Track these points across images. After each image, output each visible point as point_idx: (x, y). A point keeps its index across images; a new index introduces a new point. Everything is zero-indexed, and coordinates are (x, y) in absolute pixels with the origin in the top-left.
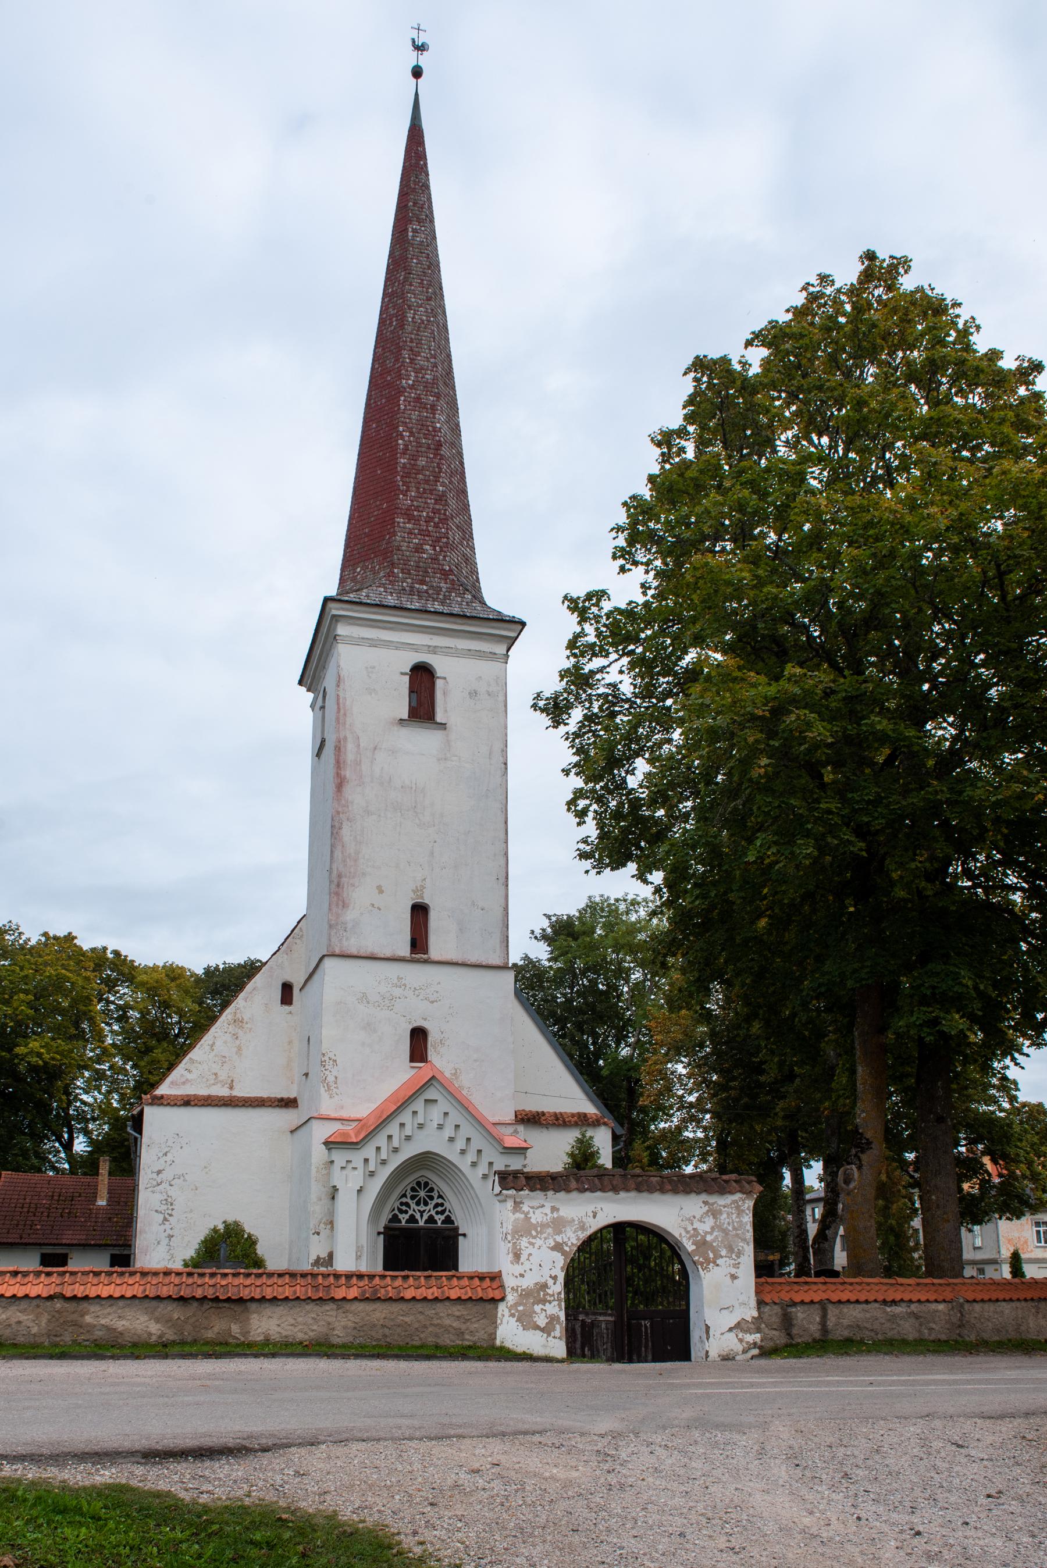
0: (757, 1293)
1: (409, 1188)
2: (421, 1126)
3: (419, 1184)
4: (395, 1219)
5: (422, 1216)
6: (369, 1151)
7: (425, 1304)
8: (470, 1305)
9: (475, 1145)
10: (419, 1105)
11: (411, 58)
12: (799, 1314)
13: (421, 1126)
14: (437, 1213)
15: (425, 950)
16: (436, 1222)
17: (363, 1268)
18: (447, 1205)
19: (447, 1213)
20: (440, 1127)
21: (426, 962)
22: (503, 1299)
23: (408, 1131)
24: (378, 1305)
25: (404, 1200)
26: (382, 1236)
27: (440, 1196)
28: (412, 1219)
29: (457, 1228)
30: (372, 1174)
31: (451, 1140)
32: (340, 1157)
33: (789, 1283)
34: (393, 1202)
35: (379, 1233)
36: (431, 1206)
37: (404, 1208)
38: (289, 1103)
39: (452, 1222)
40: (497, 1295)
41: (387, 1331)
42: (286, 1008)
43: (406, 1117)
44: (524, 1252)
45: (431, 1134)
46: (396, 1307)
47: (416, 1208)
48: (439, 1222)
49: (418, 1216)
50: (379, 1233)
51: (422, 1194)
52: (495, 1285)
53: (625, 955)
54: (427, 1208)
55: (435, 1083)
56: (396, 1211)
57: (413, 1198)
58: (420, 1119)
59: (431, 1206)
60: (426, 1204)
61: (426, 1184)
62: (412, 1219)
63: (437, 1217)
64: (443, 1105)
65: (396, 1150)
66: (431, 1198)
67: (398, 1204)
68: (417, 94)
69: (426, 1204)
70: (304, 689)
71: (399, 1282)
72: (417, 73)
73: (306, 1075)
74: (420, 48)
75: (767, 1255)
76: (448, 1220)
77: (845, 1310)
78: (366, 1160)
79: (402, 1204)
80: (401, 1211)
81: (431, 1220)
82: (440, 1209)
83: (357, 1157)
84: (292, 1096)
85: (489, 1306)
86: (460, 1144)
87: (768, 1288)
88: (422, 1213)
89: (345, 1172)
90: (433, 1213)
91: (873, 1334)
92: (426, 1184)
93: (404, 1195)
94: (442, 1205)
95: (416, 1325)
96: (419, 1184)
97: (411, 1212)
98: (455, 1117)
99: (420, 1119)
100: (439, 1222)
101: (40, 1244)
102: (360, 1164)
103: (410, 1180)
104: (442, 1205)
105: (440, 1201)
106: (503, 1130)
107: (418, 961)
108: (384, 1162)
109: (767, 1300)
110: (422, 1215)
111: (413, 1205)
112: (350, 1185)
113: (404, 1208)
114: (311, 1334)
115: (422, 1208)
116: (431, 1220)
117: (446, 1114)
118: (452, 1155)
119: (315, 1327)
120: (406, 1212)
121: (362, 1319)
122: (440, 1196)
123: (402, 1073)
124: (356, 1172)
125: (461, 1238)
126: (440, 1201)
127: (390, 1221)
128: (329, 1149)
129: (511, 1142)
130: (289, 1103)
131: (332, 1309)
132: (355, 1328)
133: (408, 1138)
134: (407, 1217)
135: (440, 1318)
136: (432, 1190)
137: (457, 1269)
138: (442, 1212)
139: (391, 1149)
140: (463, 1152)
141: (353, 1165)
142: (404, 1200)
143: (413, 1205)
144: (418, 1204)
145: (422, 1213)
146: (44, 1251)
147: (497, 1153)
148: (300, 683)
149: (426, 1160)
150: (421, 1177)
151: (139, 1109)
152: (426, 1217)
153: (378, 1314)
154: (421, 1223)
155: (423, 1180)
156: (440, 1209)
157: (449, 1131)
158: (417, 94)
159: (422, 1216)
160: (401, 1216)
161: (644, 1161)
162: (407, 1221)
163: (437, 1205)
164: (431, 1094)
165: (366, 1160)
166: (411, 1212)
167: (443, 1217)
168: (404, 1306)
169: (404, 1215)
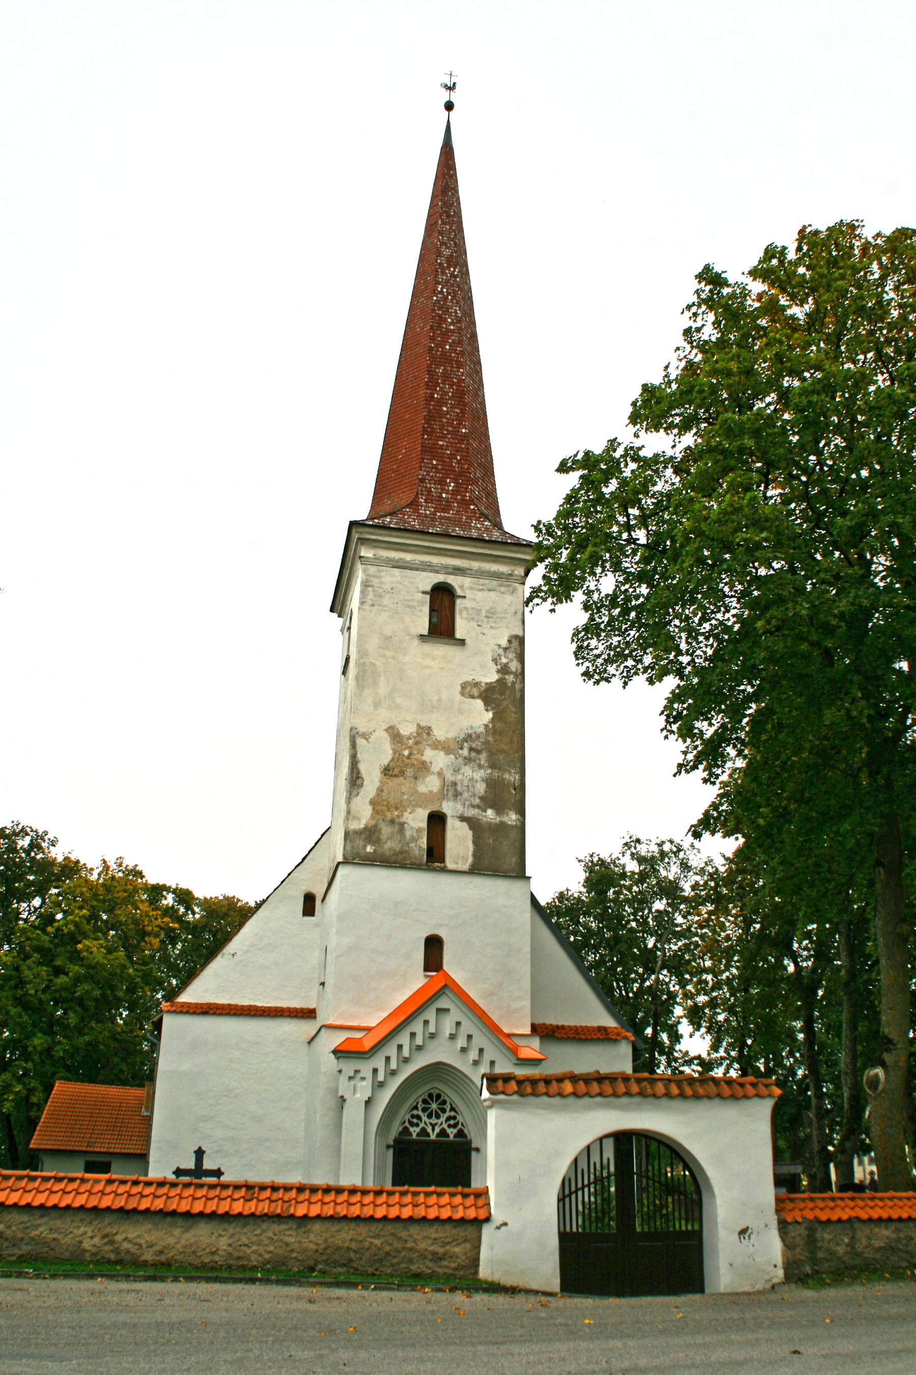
0: (778, 1211)
1: (420, 1100)
2: (432, 1036)
3: (430, 1096)
4: (406, 1131)
5: (433, 1130)
6: (378, 1062)
7: (399, 1225)
8: (448, 1227)
9: (488, 1057)
10: (430, 1014)
11: (445, 96)
12: (825, 1235)
13: (432, 1036)
14: (449, 1126)
15: (442, 860)
16: (448, 1136)
17: (370, 1184)
18: (459, 1118)
19: (460, 1126)
20: (453, 1037)
21: (444, 870)
22: (488, 1219)
23: (419, 1041)
24: (344, 1225)
25: (415, 1112)
26: (391, 1151)
27: (452, 1109)
28: (424, 1132)
29: (470, 1142)
30: (381, 1085)
31: (464, 1050)
32: (349, 1067)
33: (833, 1199)
34: (403, 1114)
35: (388, 1147)
36: (443, 1118)
37: (415, 1121)
38: (309, 1014)
39: (465, 1136)
40: (482, 1215)
41: (352, 1255)
42: (308, 919)
43: (417, 1027)
44: (528, 1167)
45: (446, 1044)
46: (363, 1229)
47: (427, 1121)
48: (452, 1137)
49: (429, 1130)
50: (388, 1147)
51: (434, 1106)
52: (480, 1202)
53: (110, 1011)
54: (440, 1121)
55: (447, 991)
56: (407, 1124)
57: (424, 1110)
58: (432, 1029)
59: (443, 1118)
60: (438, 1117)
61: (438, 1096)
62: (424, 1132)
63: (449, 1131)
64: (456, 1014)
65: (406, 1060)
66: (444, 1111)
67: (408, 1116)
68: (448, 121)
69: (438, 1117)
70: (335, 615)
71: (458, 1199)
72: (449, 106)
73: (323, 984)
74: (451, 88)
75: (803, 1173)
76: (461, 1133)
77: (877, 1230)
78: (375, 1071)
79: (413, 1116)
80: (412, 1124)
81: (443, 1133)
82: (452, 1122)
83: (366, 1069)
84: (312, 1007)
85: (470, 1230)
86: (473, 1055)
87: (789, 1205)
88: (433, 1126)
89: (352, 1083)
90: (445, 1126)
91: (908, 1257)
92: (438, 1096)
93: (416, 1108)
94: (454, 1118)
95: (387, 1248)
96: (430, 1096)
97: (422, 1125)
98: (468, 1026)
99: (432, 1029)
100: (452, 1137)
101: (85, 1152)
102: (369, 1074)
103: (421, 1093)
104: (454, 1118)
105: (453, 1114)
106: (519, 1042)
107: (434, 870)
108: (394, 1073)
109: (789, 1219)
110: (434, 1128)
111: (425, 1118)
112: (358, 1095)
113: (415, 1121)
114: (267, 1256)
115: (434, 1120)
116: (443, 1133)
117: (458, 1024)
118: (466, 1069)
119: (272, 1248)
120: (417, 1125)
121: (326, 1240)
122: (452, 1109)
123: (417, 980)
124: (364, 1083)
125: (473, 1154)
126: (453, 1114)
127: (401, 1133)
128: (338, 1058)
129: (525, 1053)
130: (309, 1014)
131: (291, 1228)
132: (317, 1251)
133: (419, 1048)
134: (418, 1130)
135: (415, 1241)
136: (444, 1102)
137: (468, 1184)
138: (455, 1126)
139: (401, 1059)
140: (476, 1063)
141: (362, 1075)
142: (415, 1112)
143: (425, 1118)
144: (430, 1116)
145: (433, 1126)
146: (89, 1159)
147: (511, 1065)
148: (332, 610)
149: (438, 1071)
150: (433, 1088)
151: (159, 1016)
152: (437, 1130)
153: (343, 1235)
154: (433, 1137)
155: (435, 1092)
156: (452, 1122)
157: (461, 1042)
158: (448, 121)
159: (433, 1130)
160: (411, 1129)
161: (650, 1072)
162: (418, 1135)
163: (449, 1118)
164: (443, 1003)
165: (375, 1071)
166: (422, 1125)
167: (455, 1131)
168: (375, 1228)
169: (415, 1128)
